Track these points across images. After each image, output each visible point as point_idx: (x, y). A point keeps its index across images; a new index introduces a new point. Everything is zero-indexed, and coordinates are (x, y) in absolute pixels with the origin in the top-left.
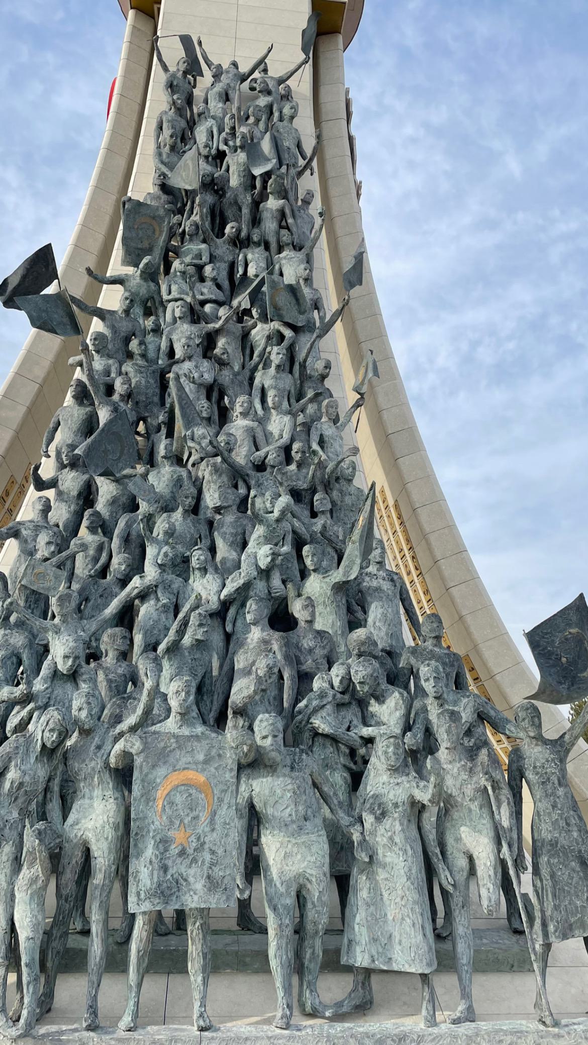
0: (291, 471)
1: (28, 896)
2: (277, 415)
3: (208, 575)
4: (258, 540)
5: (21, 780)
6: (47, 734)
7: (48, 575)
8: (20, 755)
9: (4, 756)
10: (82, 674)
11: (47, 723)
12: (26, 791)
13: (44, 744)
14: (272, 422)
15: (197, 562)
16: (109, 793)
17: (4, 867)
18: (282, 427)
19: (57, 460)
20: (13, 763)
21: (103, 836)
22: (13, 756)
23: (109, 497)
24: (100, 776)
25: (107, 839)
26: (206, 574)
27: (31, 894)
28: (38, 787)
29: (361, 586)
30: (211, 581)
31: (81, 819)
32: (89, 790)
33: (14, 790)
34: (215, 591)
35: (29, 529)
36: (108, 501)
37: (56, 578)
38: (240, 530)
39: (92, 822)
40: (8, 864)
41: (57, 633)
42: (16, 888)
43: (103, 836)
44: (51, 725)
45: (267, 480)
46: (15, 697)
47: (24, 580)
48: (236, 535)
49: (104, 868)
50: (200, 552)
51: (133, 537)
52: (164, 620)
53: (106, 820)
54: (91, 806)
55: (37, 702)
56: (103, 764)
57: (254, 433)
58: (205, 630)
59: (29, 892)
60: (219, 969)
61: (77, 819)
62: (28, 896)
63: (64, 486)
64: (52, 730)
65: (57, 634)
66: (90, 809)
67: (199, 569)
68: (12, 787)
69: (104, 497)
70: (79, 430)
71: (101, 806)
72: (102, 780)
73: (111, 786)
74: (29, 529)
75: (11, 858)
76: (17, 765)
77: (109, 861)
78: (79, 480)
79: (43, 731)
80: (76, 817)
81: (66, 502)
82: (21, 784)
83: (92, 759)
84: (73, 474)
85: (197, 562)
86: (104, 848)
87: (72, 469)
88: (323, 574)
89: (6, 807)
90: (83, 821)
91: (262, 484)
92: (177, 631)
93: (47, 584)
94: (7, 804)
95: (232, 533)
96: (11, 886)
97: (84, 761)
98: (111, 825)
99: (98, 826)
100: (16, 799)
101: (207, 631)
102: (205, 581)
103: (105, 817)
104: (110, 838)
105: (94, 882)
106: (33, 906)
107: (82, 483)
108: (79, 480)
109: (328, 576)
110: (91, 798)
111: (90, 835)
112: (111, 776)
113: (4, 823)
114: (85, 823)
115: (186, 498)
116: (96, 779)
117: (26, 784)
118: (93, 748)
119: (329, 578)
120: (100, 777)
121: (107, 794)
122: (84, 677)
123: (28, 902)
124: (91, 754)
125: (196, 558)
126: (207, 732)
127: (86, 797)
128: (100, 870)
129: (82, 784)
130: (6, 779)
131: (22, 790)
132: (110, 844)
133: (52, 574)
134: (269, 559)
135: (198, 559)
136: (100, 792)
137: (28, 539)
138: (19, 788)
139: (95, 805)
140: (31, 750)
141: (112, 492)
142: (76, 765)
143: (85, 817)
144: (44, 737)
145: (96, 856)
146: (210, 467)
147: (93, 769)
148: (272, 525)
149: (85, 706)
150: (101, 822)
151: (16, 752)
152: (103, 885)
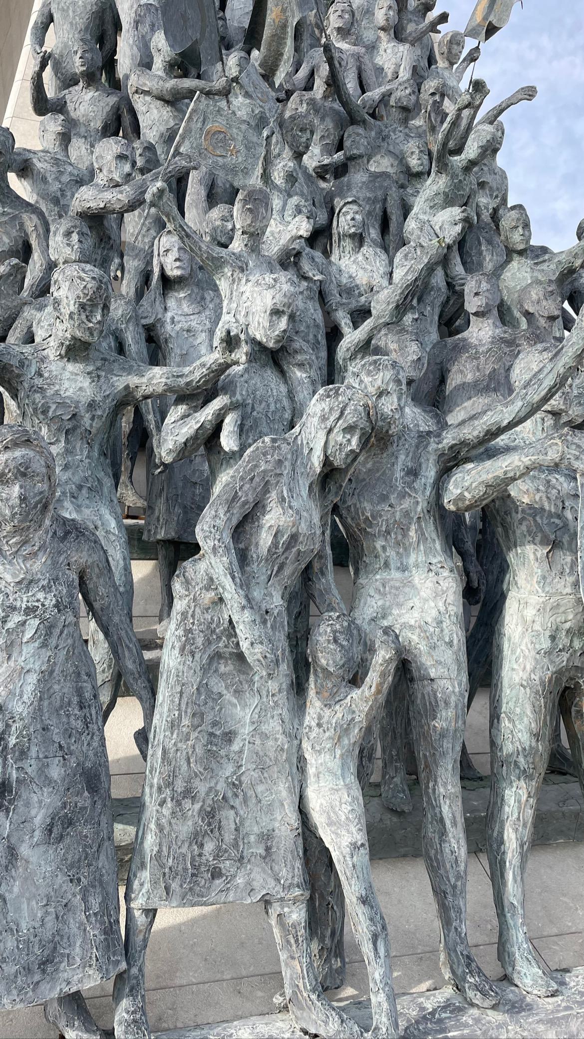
0: (417, 128)
1: (338, 761)
2: (388, 42)
3: (364, 249)
4: (433, 199)
5: (294, 530)
6: (338, 437)
7: (233, 139)
8: (284, 479)
9: (257, 479)
10: (296, 352)
11: (342, 413)
12: (299, 552)
13: (326, 457)
14: (382, 52)
15: (351, 223)
16: (438, 558)
17: (276, 703)
18: (399, 60)
19: (56, 76)
20: (273, 495)
21: (440, 638)
22: (273, 481)
23: (163, 129)
24: (420, 526)
25: (450, 644)
26: (361, 245)
27: (342, 756)
28: (314, 544)
29: (576, 284)
30: (371, 258)
31: (390, 607)
32: (398, 553)
33: (281, 550)
34: (381, 272)
35: (46, 161)
36: (162, 135)
37: (248, 148)
38: (380, 194)
39: (416, 614)
40: (282, 698)
41: (242, 270)
42: (306, 745)
43: (440, 638)
44: (350, 418)
45: (394, 131)
46: (188, 384)
47: (187, 143)
48: (374, 201)
49: (453, 699)
50: (355, 207)
51: (219, 190)
52: (312, 311)
53: (442, 609)
54: (409, 583)
55: (233, 394)
56: (426, 504)
57: (361, 62)
58: (416, 316)
59: (338, 752)
60: (549, 840)
61: (383, 608)
62: (337, 760)
63: (78, 113)
64: (349, 429)
65: (243, 271)
66: (407, 590)
67: (352, 236)
68: (275, 544)
69: (155, 128)
70: (87, 28)
71: (429, 584)
72: (423, 534)
73: (438, 546)
74: (46, 161)
75: (284, 686)
76: (283, 500)
77: (460, 685)
78: (102, 104)
79: (330, 431)
80: (380, 603)
81: (85, 137)
82: (294, 538)
83: (403, 495)
84: (90, 94)
85: (351, 223)
86: (449, 661)
87: (89, 85)
88: (533, 259)
89: (262, 585)
90: (395, 612)
91: (388, 136)
92: (397, 306)
93: (231, 160)
94: (264, 578)
95: (369, 199)
96: (296, 742)
97: (384, 498)
98: (454, 619)
99: (429, 620)
100: (281, 568)
101: (416, 320)
102: (360, 257)
103: (441, 604)
104: (455, 642)
105: (439, 724)
106: (348, 781)
107: (108, 109)
108: (102, 104)
109: (544, 261)
110: (404, 568)
111: (415, 638)
112: (436, 528)
113: (262, 616)
114: (399, 616)
115: (301, 131)
116: (412, 533)
117: (301, 539)
118: (399, 474)
119: (547, 264)
120: (421, 532)
121: (434, 561)
122: (299, 358)
123: (339, 772)
124: (400, 485)
125: (349, 217)
126: (541, 457)
127: (392, 566)
128: (447, 703)
129: (379, 544)
130: (260, 527)
131: (294, 550)
132: (456, 653)
133: (240, 138)
134: (458, 228)
135: (353, 219)
136: (421, 558)
137: (48, 175)
138: (288, 546)
139: (416, 581)
140: (300, 470)
141: (167, 122)
142: (367, 506)
143: (400, 605)
144: (332, 443)
145: (432, 675)
146: (305, 105)
147: (407, 514)
148: (457, 175)
149: (391, 387)
150: (434, 613)
151: (278, 471)
152: (456, 731)
